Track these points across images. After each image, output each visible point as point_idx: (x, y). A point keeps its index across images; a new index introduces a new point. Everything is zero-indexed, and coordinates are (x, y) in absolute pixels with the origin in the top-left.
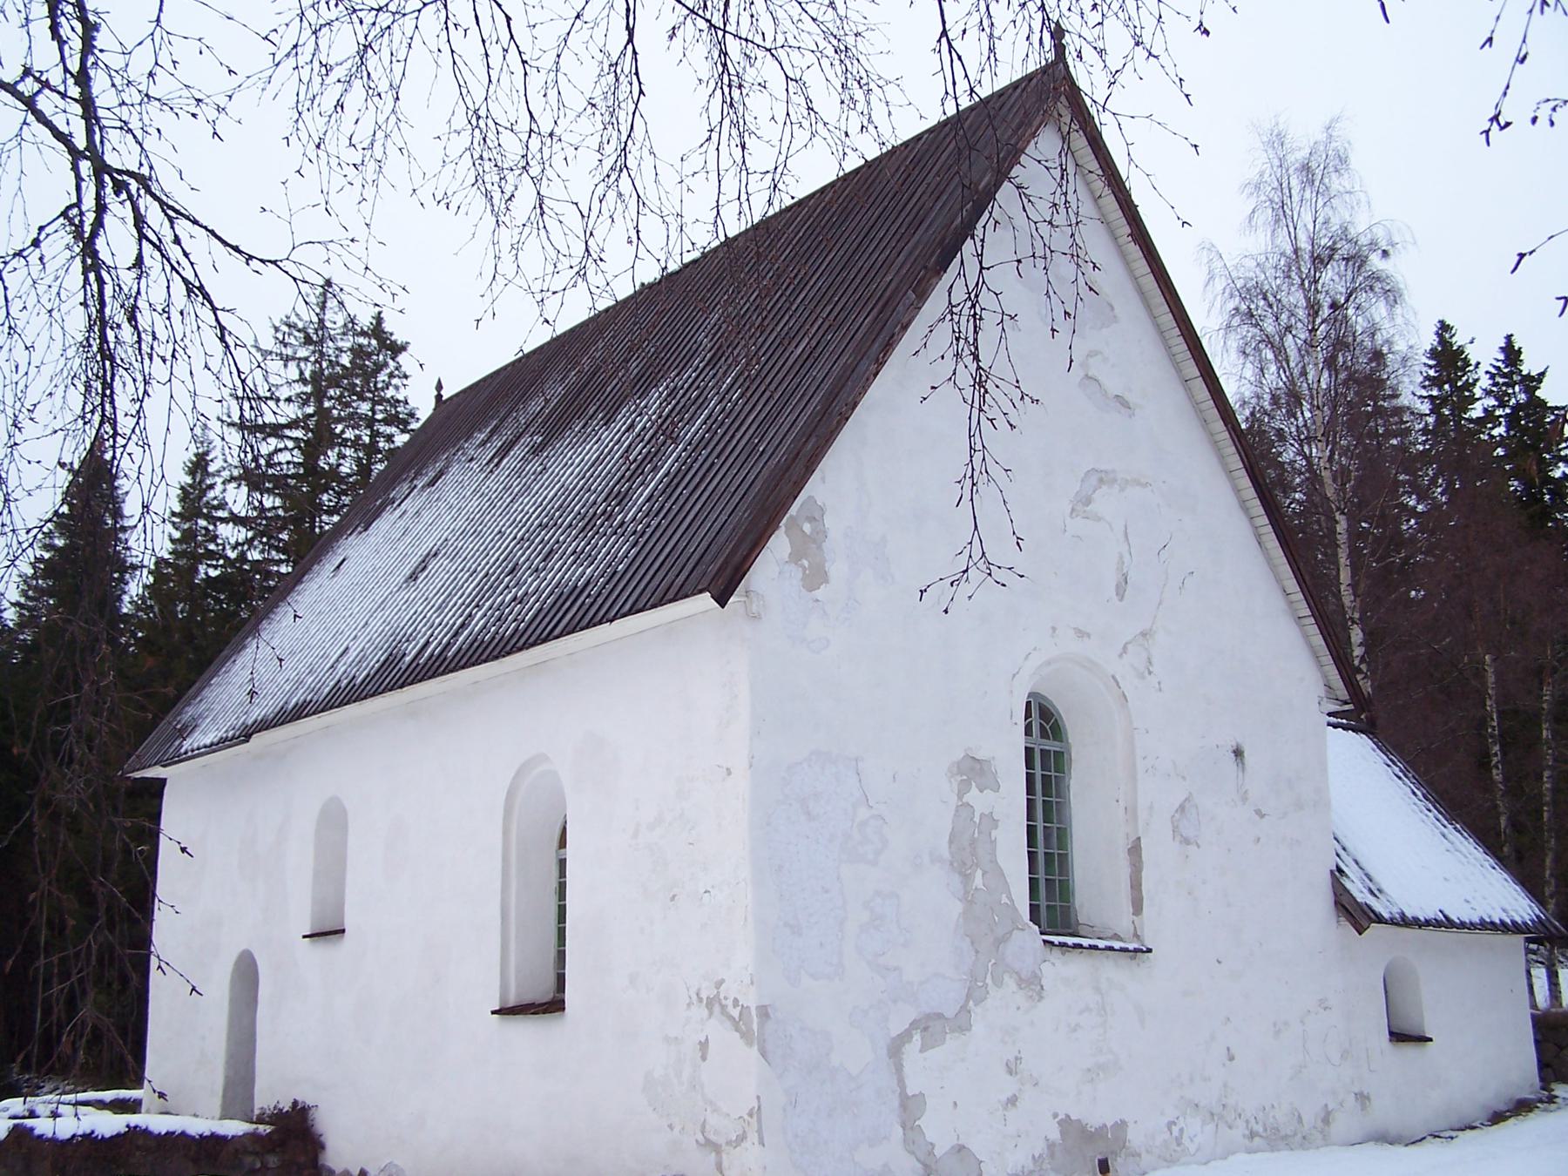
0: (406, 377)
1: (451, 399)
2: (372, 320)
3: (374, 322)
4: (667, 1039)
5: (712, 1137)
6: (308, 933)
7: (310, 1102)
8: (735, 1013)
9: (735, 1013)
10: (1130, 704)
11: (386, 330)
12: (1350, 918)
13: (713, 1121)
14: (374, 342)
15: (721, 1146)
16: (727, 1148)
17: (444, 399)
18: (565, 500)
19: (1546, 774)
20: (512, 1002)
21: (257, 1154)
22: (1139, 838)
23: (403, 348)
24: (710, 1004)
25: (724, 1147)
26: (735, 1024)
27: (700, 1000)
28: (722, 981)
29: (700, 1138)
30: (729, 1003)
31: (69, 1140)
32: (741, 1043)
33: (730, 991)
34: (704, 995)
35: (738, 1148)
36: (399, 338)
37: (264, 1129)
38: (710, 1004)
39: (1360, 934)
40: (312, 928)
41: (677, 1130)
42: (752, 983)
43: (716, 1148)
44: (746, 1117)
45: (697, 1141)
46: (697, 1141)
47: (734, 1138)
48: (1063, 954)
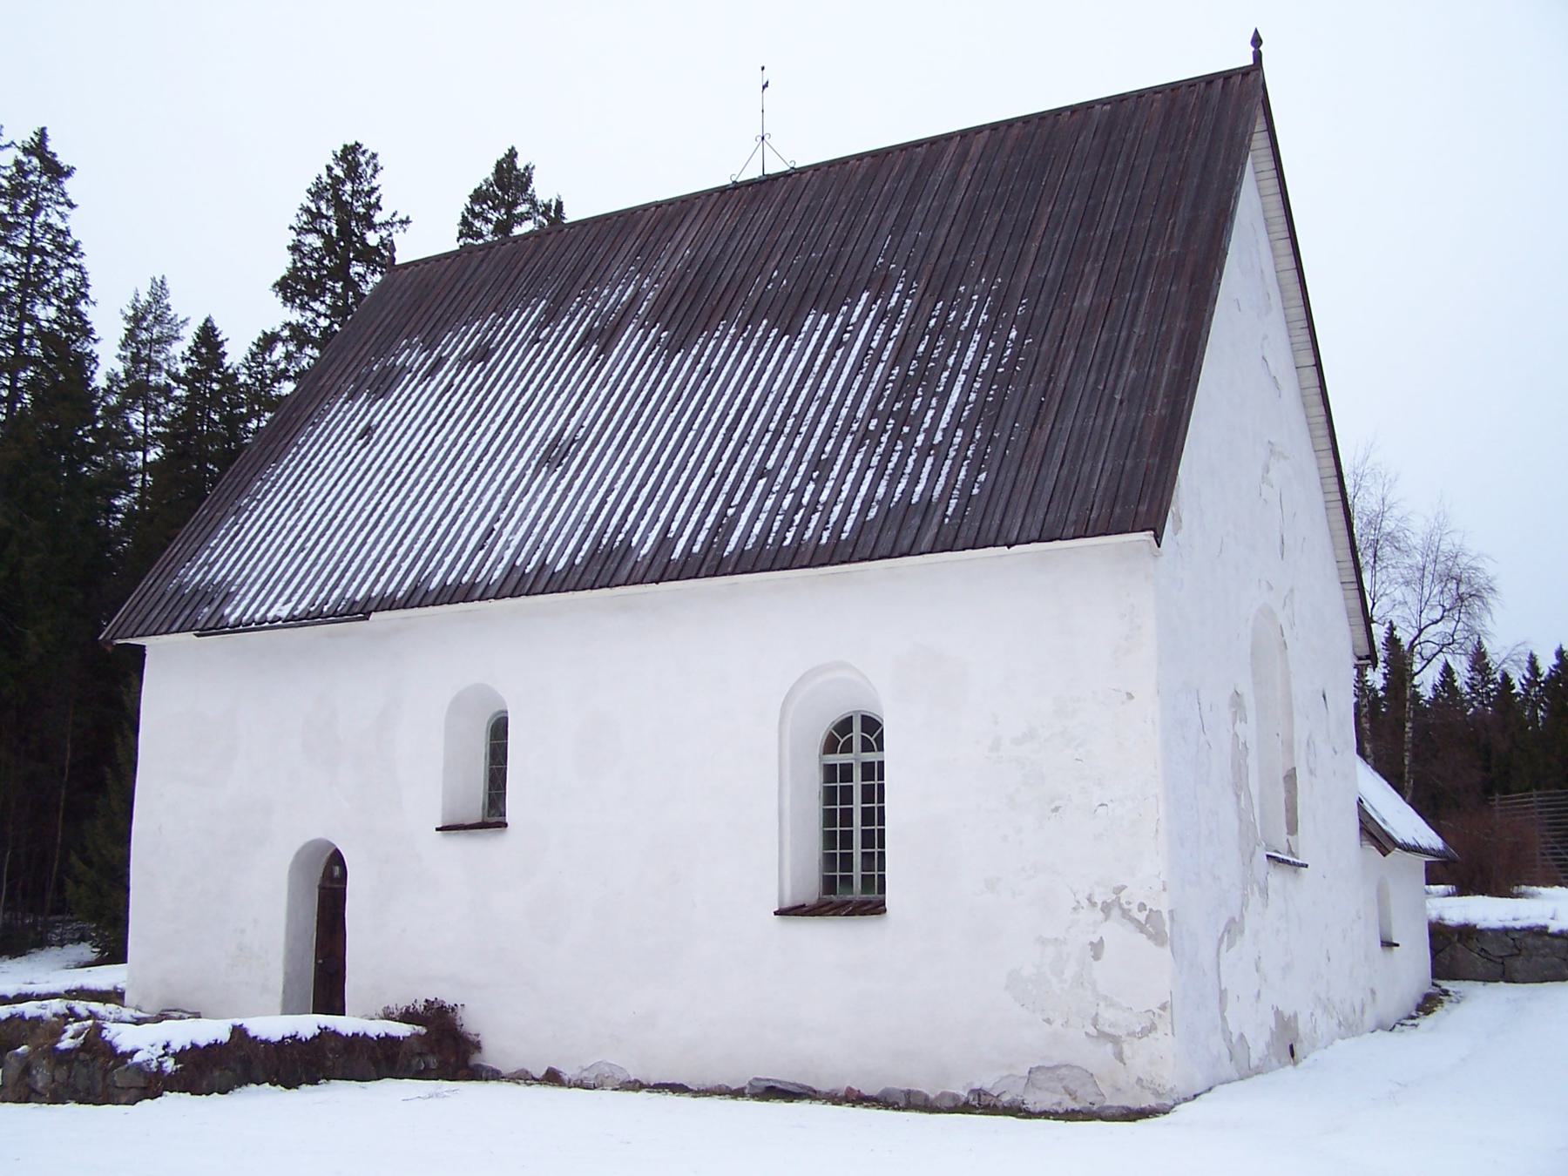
0: (71, 206)
1: (406, 266)
2: (33, 136)
3: (36, 139)
4: (1043, 942)
5: (1107, 1029)
6: (440, 826)
7: (449, 1002)
8: (1142, 917)
9: (1142, 917)
10: (1289, 651)
11: (49, 149)
12: (1375, 842)
13: (1107, 1015)
14: (35, 161)
15: (1121, 1037)
16: (1128, 1038)
17: (397, 263)
18: (772, 413)
19: (1409, 725)
20: (788, 904)
21: (420, 1054)
22: (1294, 769)
23: (68, 173)
24: (1106, 908)
25: (1124, 1038)
26: (1141, 928)
27: (1093, 904)
28: (1124, 887)
29: (1093, 1031)
30: (1134, 908)
31: (279, 1042)
32: (1150, 944)
33: (1134, 895)
34: (1098, 900)
35: (1145, 1039)
36: (63, 160)
37: (402, 1030)
38: (1106, 908)
39: (1384, 855)
40: (443, 816)
41: (1057, 1025)
42: (1164, 890)
43: (1115, 1040)
44: (1157, 1011)
45: (1087, 1034)
46: (1087, 1034)
47: (1139, 1029)
48: (1275, 865)
